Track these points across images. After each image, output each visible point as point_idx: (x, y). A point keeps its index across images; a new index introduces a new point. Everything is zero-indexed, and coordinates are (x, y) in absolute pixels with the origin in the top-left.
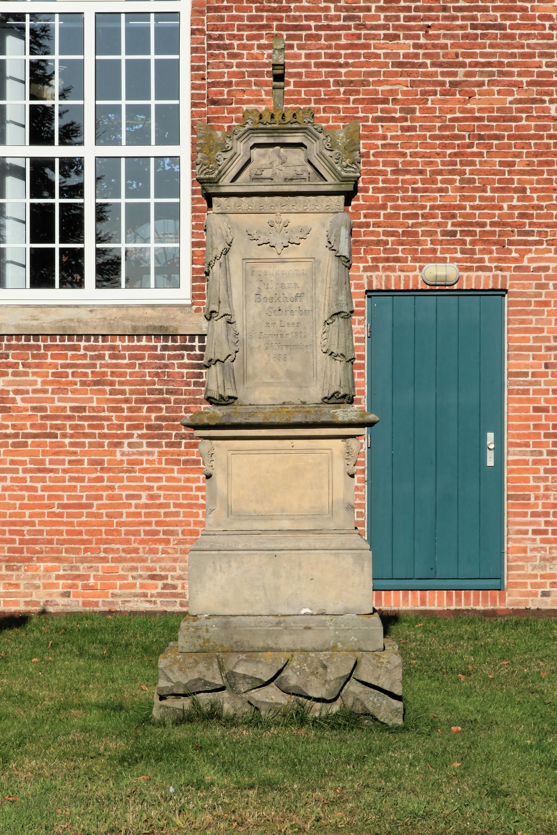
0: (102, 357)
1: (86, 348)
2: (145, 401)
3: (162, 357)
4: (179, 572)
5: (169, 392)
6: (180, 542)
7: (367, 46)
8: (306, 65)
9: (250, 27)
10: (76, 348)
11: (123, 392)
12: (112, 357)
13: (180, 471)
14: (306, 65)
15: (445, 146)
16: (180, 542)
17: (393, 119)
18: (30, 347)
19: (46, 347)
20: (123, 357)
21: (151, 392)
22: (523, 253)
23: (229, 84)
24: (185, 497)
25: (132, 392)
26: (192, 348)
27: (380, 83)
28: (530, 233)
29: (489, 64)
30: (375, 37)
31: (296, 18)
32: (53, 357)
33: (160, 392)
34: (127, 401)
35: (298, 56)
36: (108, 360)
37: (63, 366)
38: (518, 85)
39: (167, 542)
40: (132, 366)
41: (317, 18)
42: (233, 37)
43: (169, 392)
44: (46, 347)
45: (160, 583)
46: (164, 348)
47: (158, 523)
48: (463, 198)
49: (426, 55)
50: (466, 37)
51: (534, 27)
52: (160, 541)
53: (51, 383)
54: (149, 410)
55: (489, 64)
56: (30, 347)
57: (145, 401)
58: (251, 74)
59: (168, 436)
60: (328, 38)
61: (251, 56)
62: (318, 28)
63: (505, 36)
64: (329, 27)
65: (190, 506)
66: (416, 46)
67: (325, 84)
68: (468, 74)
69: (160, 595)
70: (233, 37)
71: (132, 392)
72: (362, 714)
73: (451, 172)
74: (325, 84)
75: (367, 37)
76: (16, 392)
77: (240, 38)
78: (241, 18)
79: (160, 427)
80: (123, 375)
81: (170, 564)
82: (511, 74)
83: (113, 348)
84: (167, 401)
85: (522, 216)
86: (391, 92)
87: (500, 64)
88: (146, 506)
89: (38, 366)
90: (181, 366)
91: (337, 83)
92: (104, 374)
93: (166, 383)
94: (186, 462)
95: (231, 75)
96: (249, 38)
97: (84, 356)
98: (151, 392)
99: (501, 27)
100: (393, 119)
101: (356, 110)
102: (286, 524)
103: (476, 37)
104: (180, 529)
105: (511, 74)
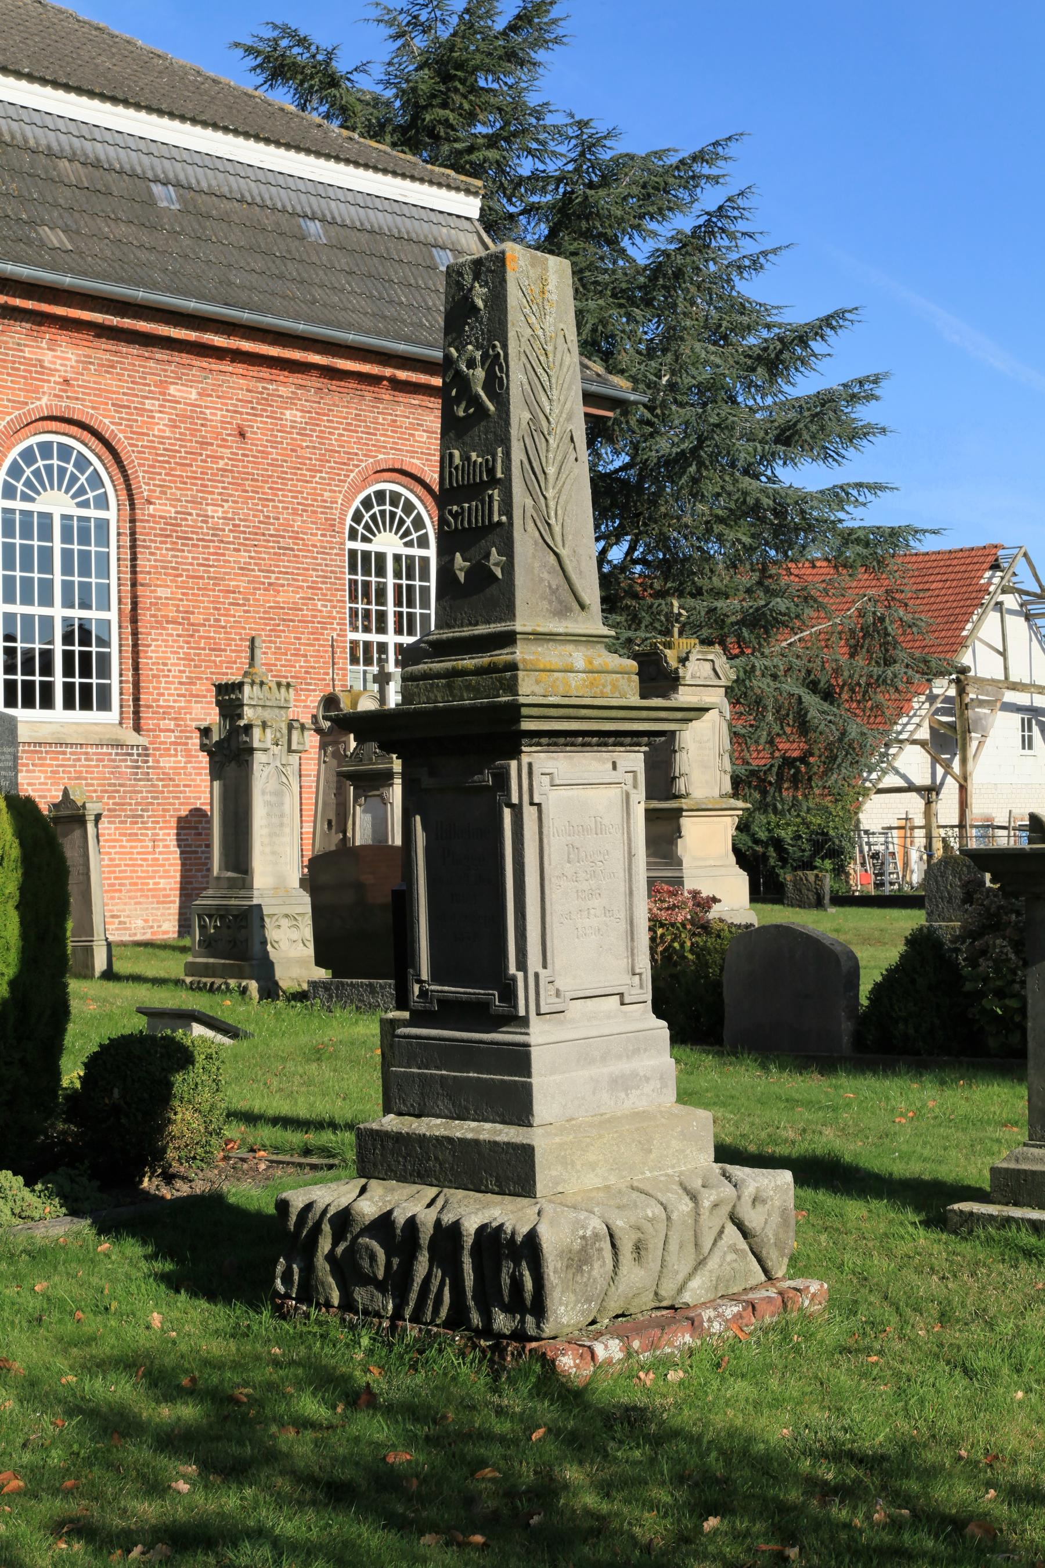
0: (79, 760)
1: (71, 753)
2: (106, 791)
3: (114, 761)
4: (127, 913)
5: (121, 785)
6: (129, 891)
7: (223, 555)
8: (192, 564)
9: (161, 535)
10: (64, 753)
11: (92, 785)
12: (86, 760)
13: (128, 841)
14: (192, 564)
15: (266, 625)
16: (129, 891)
17: (238, 605)
18: (36, 752)
19: (47, 752)
20: (91, 760)
21: (110, 785)
22: (307, 696)
23: (149, 573)
24: (131, 859)
25: (99, 785)
26: (132, 755)
27: (230, 580)
28: (310, 684)
29: (287, 573)
30: (228, 549)
31: (186, 532)
32: (51, 759)
33: (114, 785)
34: (95, 791)
35: (187, 558)
36: (84, 762)
37: (58, 766)
38: (301, 587)
39: (120, 891)
40: (97, 766)
41: (197, 533)
42: (151, 541)
43: (121, 785)
44: (47, 752)
45: (117, 921)
46: (117, 754)
47: (116, 878)
48: (277, 659)
49: (256, 564)
50: (275, 554)
51: (309, 551)
52: (116, 891)
53: (49, 778)
54: (109, 798)
55: (287, 573)
56: (36, 752)
57: (106, 791)
58: (163, 567)
59: (120, 816)
60: (204, 547)
61: (161, 555)
62: (199, 540)
63: (295, 556)
64: (203, 540)
65: (133, 865)
66: (250, 557)
67: (202, 578)
68: (277, 578)
69: (117, 929)
70: (151, 541)
71: (99, 785)
72: (599, 351)
73: (270, 642)
74: (202, 578)
75: (225, 548)
76: (29, 784)
77: (155, 542)
78: (155, 529)
79: (115, 810)
80: (92, 773)
81: (122, 907)
82: (297, 580)
83: (87, 753)
84: (118, 791)
85: (307, 672)
86: (238, 586)
87: (292, 574)
88: (108, 866)
89: (42, 765)
90: (127, 767)
91: (209, 578)
92: (81, 772)
93: (118, 778)
94: (130, 834)
95: (151, 567)
96: (161, 542)
97: (69, 759)
98: (110, 785)
99: (292, 550)
100: (238, 605)
101: (218, 597)
102: (712, 863)
103: (280, 554)
104: (127, 882)
105: (297, 580)
